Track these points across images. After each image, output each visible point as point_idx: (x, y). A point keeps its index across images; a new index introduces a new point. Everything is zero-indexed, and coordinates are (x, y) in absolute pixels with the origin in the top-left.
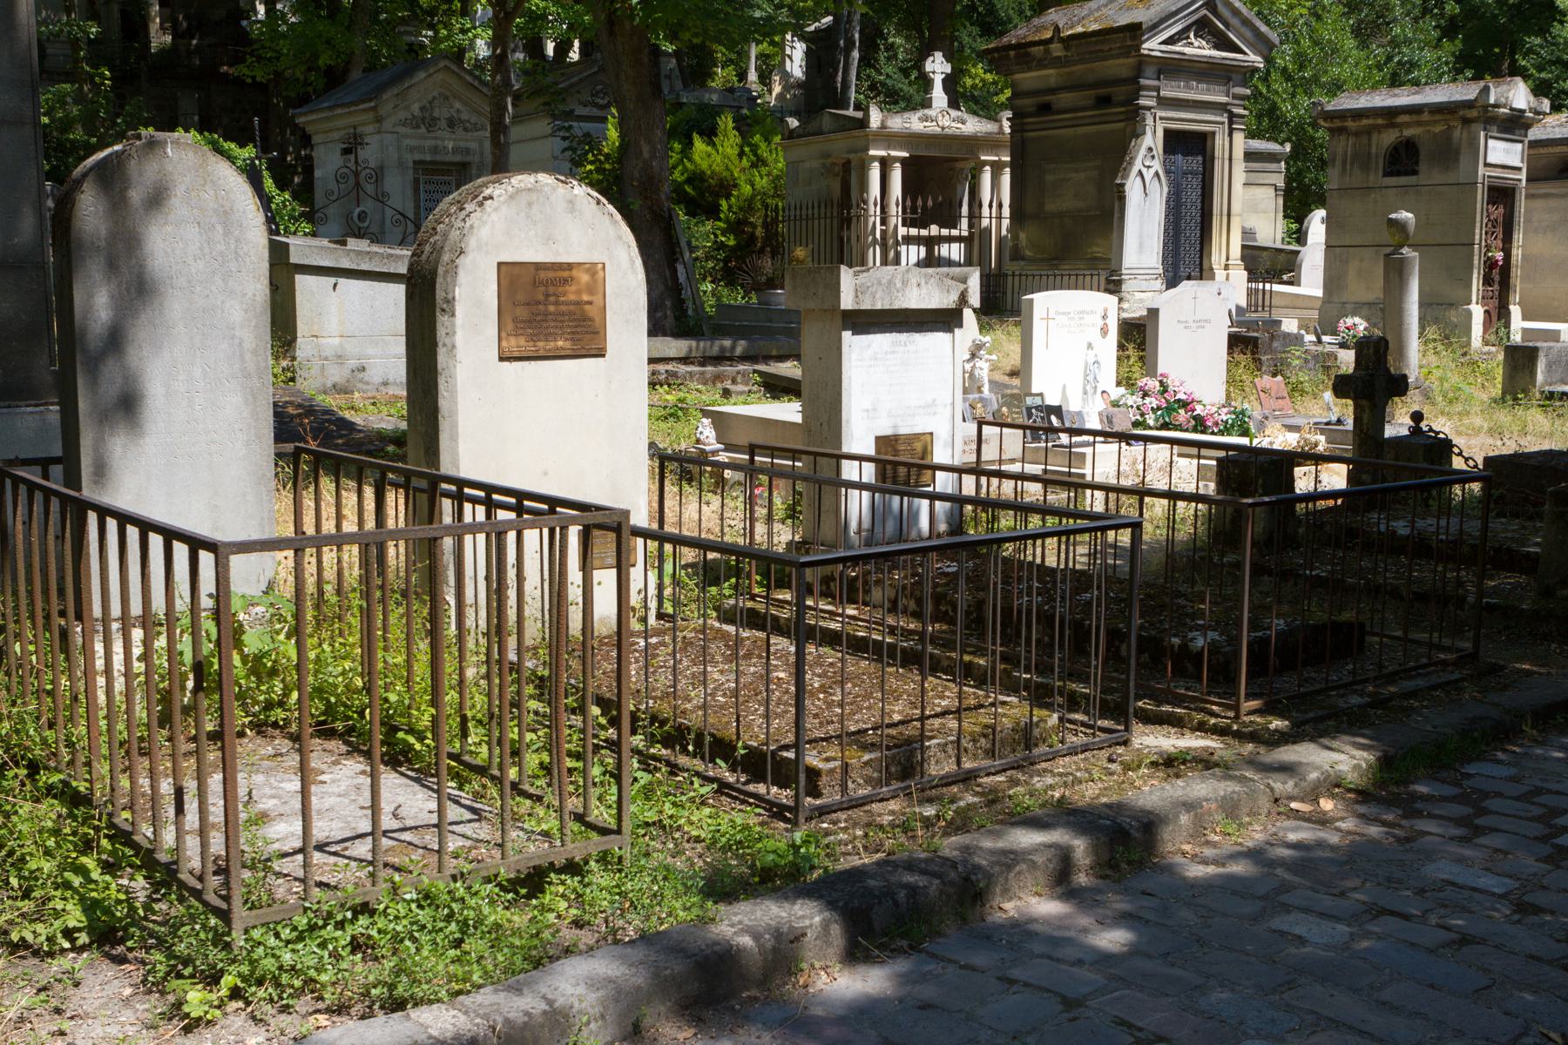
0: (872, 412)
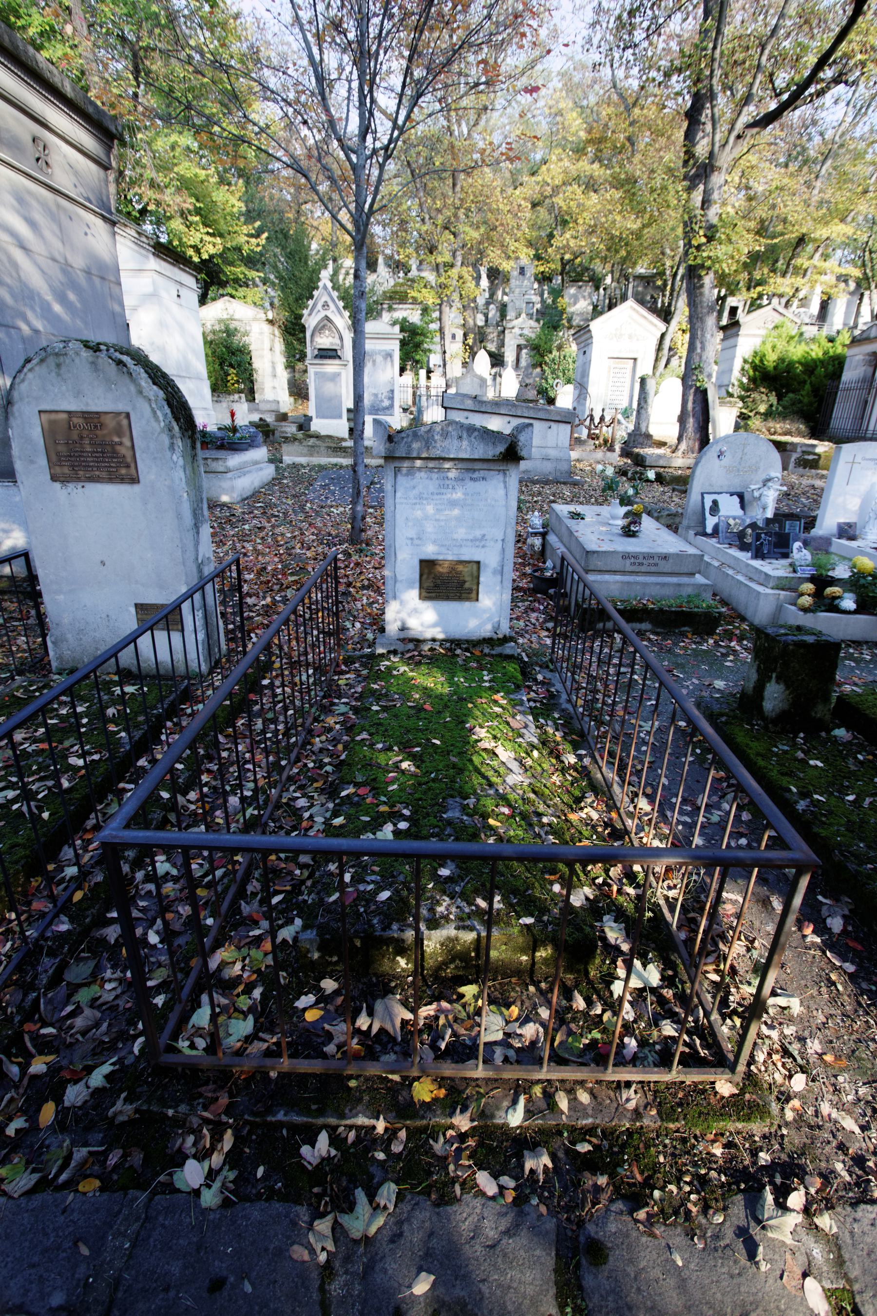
0: (417, 540)
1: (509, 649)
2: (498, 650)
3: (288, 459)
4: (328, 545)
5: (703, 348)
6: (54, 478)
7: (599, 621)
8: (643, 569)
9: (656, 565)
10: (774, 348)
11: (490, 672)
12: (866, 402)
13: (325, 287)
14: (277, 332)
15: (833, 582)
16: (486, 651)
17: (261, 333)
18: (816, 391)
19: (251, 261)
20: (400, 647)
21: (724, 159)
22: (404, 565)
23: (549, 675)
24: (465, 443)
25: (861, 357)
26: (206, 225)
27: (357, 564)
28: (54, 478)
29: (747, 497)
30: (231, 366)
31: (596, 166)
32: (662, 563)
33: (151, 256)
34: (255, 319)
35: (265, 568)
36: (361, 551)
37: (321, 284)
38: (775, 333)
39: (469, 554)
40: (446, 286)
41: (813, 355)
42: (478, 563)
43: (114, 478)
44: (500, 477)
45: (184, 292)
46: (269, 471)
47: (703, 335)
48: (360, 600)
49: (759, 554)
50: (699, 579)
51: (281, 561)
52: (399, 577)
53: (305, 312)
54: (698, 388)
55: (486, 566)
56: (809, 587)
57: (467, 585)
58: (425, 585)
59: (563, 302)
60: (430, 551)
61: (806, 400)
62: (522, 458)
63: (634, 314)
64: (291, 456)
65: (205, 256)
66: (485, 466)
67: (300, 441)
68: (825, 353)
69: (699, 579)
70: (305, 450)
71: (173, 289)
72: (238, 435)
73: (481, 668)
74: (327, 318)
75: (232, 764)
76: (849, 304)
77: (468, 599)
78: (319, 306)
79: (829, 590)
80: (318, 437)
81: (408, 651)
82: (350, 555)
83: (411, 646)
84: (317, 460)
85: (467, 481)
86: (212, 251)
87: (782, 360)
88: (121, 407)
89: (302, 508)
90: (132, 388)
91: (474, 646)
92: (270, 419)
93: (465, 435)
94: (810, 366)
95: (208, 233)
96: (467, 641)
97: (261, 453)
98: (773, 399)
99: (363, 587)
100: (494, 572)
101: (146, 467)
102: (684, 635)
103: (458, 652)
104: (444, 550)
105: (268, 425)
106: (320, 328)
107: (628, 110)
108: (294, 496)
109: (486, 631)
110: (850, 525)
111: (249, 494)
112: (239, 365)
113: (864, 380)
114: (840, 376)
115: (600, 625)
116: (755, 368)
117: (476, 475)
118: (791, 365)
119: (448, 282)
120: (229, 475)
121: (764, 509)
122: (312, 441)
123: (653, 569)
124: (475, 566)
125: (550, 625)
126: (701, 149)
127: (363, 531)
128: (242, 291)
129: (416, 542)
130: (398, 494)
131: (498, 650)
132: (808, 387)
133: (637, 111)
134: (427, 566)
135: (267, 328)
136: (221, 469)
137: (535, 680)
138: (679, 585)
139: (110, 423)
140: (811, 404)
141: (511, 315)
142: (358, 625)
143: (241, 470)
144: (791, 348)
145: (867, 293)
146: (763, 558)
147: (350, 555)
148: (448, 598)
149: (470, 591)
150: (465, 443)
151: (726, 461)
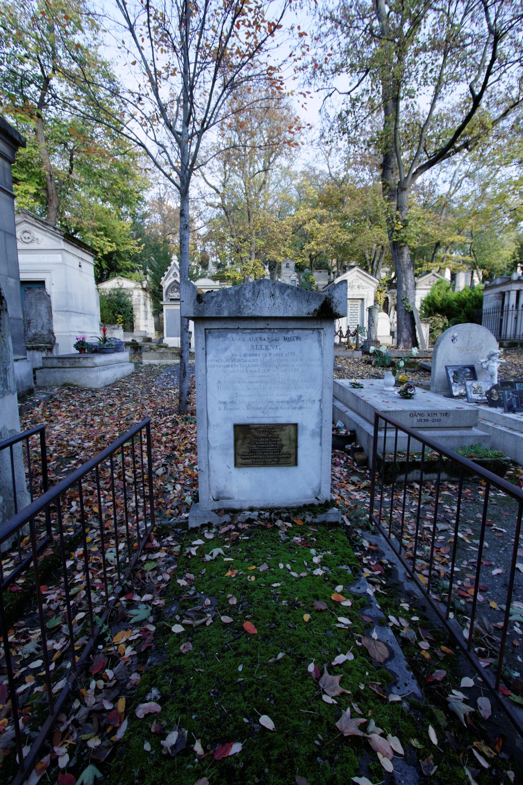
0: (230, 404)
1: (333, 515)
2: (321, 518)
3: (146, 362)
4: (160, 415)
7: (401, 473)
8: (428, 424)
9: (439, 420)
10: (439, 294)
11: (319, 548)
12: (501, 320)
13: (175, 264)
14: (148, 295)
16: (309, 519)
17: (139, 296)
19: (135, 259)
20: (215, 520)
23: (374, 539)
24: (279, 301)
25: (493, 295)
26: (106, 236)
27: (183, 430)
29: (477, 368)
30: (120, 313)
31: (324, 210)
32: (444, 418)
33: (62, 242)
34: (135, 288)
35: (104, 437)
36: (187, 419)
37: (172, 263)
39: (284, 416)
40: (247, 269)
42: (296, 425)
44: (315, 335)
45: (83, 264)
46: (130, 368)
47: (406, 281)
48: (183, 462)
49: (510, 409)
50: (476, 431)
51: (120, 430)
52: (212, 444)
53: (163, 278)
55: (304, 428)
57: (285, 449)
58: (241, 451)
59: (312, 278)
60: (244, 416)
62: (338, 316)
63: (360, 275)
64: (147, 359)
65: (106, 253)
66: (299, 325)
67: (154, 350)
68: (470, 295)
69: (476, 431)
70: (158, 356)
71: (77, 261)
72: (107, 343)
73: (307, 544)
75: (135, 541)
76: (466, 277)
77: (287, 464)
78: (171, 275)
80: (166, 347)
81: (225, 524)
82: (177, 423)
83: (227, 518)
84: (164, 362)
85: (281, 341)
86: (110, 249)
87: (444, 300)
89: (149, 390)
91: (295, 514)
92: (139, 341)
93: (277, 293)
95: (109, 241)
96: (288, 509)
97: (125, 355)
99: (187, 450)
100: (313, 434)
103: (279, 523)
104: (259, 414)
105: (137, 344)
107: (340, 186)
108: (144, 383)
111: (111, 382)
112: (124, 313)
113: (498, 308)
114: (481, 307)
115: (402, 477)
116: (430, 305)
117: (290, 334)
119: (248, 267)
120: (95, 369)
121: (492, 376)
122: (162, 350)
123: (436, 424)
124: (292, 429)
125: (355, 478)
127: (188, 403)
128: (130, 274)
129: (229, 406)
130: (209, 357)
131: (321, 518)
132: (463, 313)
133: (343, 186)
134: (242, 431)
135: (142, 293)
136: (90, 365)
137: (362, 547)
138: (462, 437)
142: (179, 487)
143: (106, 366)
144: (448, 294)
146: (514, 412)
147: (177, 423)
148: (265, 464)
149: (288, 455)
150: (279, 301)
151: (458, 343)
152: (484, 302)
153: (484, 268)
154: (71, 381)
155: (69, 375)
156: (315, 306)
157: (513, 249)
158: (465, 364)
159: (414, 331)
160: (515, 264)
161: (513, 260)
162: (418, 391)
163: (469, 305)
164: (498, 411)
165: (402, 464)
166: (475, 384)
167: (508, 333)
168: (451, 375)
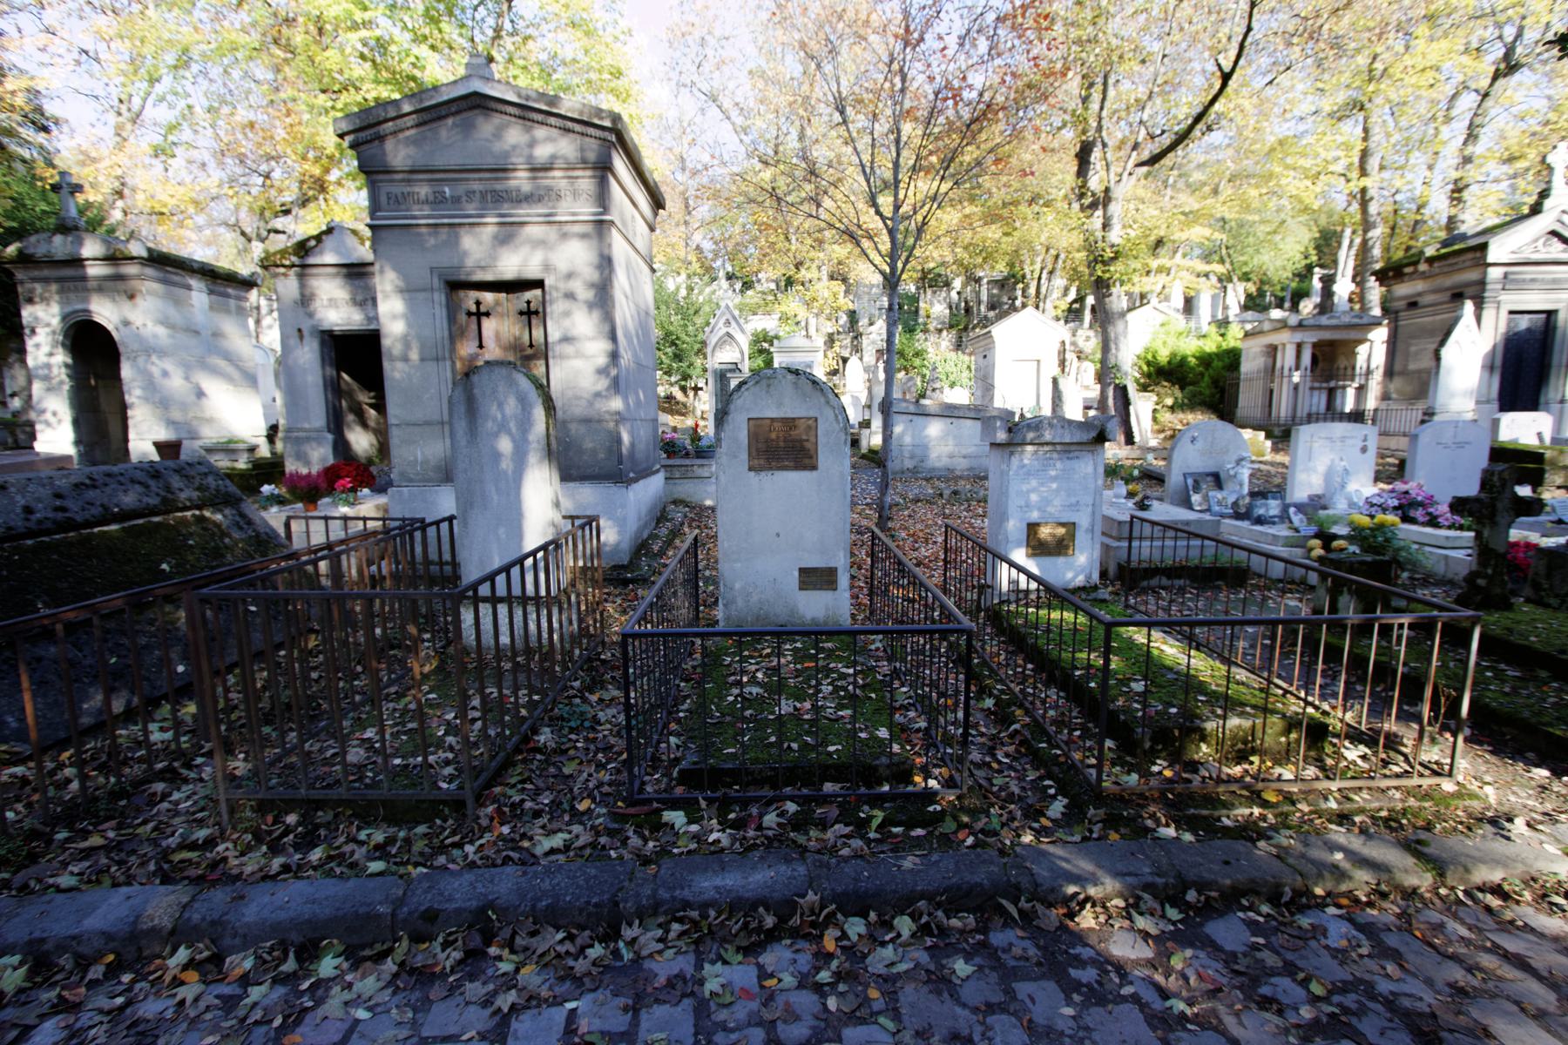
2: (1093, 595)
5: (1117, 349)
6: (750, 469)
12: (1271, 392)
15: (1335, 537)
18: (1215, 382)
21: (1118, 192)
22: (1014, 526)
25: (1258, 349)
28: (750, 469)
29: (1222, 476)
38: (1163, 330)
41: (1208, 349)
43: (800, 466)
54: (1117, 386)
56: (1316, 542)
61: (1207, 392)
68: (1219, 347)
74: (728, 334)
78: (721, 324)
79: (1335, 544)
87: (1173, 355)
88: (812, 414)
90: (822, 400)
94: (1206, 360)
98: (1179, 394)
101: (823, 458)
102: (1219, 588)
106: (720, 343)
109: (1080, 580)
110: (1319, 497)
115: (1145, 583)
116: (1148, 364)
118: (1184, 359)
121: (1241, 485)
126: (1095, 183)
132: (1206, 379)
139: (802, 425)
140: (1213, 395)
141: (863, 322)
145: (1230, 286)
151: (1199, 445)
152: (1243, 359)
153: (1248, 280)
154: (682, 496)
155: (680, 489)
156: (1093, 434)
157: (1306, 242)
158: (1207, 470)
159: (1128, 414)
160: (1309, 268)
161: (1304, 262)
162: (1155, 504)
163: (1217, 364)
164: (1245, 524)
165: (1146, 570)
166: (1219, 495)
167: (1283, 414)
168: (1190, 481)
